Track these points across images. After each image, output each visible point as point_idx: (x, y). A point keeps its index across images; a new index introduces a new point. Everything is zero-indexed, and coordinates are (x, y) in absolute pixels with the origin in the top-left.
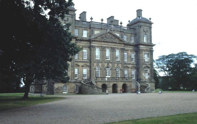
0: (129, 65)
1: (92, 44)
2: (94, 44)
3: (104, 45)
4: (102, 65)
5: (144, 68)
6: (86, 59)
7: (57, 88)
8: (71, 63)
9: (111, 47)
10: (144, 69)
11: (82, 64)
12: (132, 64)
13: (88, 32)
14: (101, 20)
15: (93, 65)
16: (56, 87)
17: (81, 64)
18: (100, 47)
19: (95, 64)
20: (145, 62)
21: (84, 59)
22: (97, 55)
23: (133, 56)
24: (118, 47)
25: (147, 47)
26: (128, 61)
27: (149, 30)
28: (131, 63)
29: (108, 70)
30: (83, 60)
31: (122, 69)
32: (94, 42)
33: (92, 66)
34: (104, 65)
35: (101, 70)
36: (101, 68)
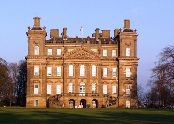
0: (53, 80)
1: (65, 62)
2: (67, 61)
3: (77, 61)
4: (75, 81)
5: (125, 83)
6: (60, 76)
7: (29, 102)
8: (42, 80)
9: (86, 64)
10: (124, 85)
11: (56, 80)
12: (113, 79)
13: (63, 50)
14: (28, 28)
15: (66, 81)
16: (28, 101)
17: (54, 80)
18: (74, 64)
19: (68, 80)
20: (126, 77)
21: (57, 76)
22: (35, 71)
23: (115, 70)
24: (94, 63)
25: (129, 61)
26: (108, 76)
27: (133, 42)
28: (112, 78)
29: (82, 86)
30: (57, 77)
31: (99, 84)
32: (67, 60)
33: (64, 82)
34: (78, 81)
35: (74, 86)
36: (74, 84)
